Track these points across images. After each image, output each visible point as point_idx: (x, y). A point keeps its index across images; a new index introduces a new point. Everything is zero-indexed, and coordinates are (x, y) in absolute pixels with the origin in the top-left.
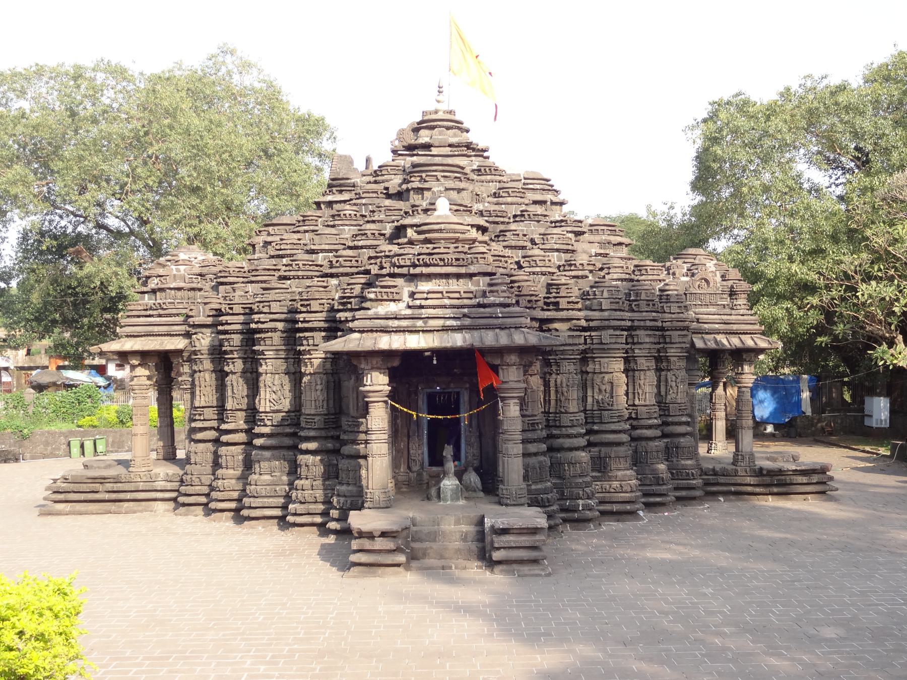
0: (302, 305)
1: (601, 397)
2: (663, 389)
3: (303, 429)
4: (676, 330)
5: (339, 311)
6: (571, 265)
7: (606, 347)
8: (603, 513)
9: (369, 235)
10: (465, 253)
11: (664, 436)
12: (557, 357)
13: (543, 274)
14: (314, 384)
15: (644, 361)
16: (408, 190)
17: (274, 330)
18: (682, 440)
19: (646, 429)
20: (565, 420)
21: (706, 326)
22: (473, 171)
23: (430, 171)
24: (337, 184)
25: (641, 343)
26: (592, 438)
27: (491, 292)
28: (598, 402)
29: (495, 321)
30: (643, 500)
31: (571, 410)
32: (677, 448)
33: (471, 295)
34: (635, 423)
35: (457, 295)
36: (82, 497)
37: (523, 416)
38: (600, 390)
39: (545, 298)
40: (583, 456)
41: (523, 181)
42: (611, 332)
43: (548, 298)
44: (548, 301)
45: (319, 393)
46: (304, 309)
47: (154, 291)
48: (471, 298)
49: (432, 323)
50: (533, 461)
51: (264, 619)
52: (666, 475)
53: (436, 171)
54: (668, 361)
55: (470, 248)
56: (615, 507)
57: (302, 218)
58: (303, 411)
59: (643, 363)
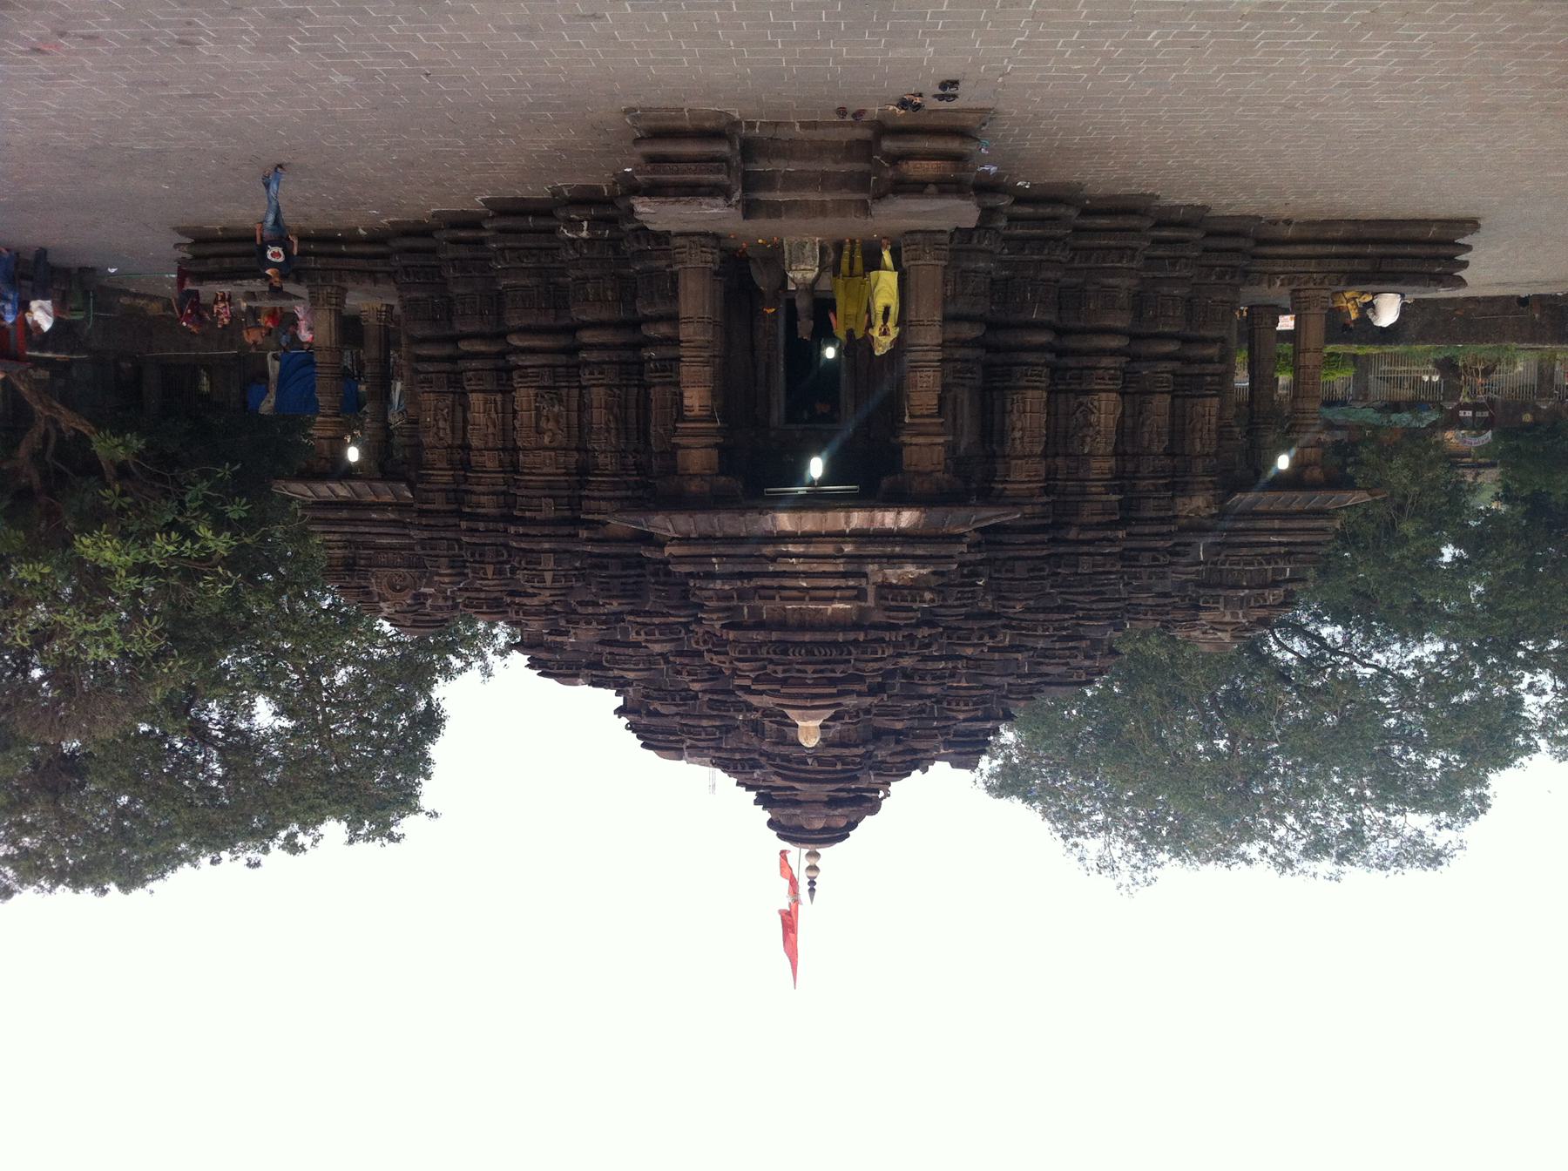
1: (556, 409)
2: (459, 415)
3: (1047, 365)
4: (438, 511)
5: (981, 562)
7: (547, 492)
9: (928, 677)
10: (771, 661)
13: (649, 614)
15: (488, 464)
16: (865, 742)
17: (1084, 527)
19: (482, 353)
22: (761, 767)
23: (829, 772)
25: (493, 493)
27: (729, 598)
28: (560, 401)
29: (722, 550)
30: (483, 234)
31: (602, 390)
32: (435, 320)
33: (762, 592)
34: (501, 363)
36: (1409, 250)
37: (677, 384)
38: (558, 422)
42: (539, 516)
44: (639, 571)
45: (1019, 425)
47: (1275, 584)
48: (764, 587)
49: (829, 549)
50: (662, 309)
51: (1148, 34)
53: (820, 772)
54: (450, 462)
59: (490, 461)
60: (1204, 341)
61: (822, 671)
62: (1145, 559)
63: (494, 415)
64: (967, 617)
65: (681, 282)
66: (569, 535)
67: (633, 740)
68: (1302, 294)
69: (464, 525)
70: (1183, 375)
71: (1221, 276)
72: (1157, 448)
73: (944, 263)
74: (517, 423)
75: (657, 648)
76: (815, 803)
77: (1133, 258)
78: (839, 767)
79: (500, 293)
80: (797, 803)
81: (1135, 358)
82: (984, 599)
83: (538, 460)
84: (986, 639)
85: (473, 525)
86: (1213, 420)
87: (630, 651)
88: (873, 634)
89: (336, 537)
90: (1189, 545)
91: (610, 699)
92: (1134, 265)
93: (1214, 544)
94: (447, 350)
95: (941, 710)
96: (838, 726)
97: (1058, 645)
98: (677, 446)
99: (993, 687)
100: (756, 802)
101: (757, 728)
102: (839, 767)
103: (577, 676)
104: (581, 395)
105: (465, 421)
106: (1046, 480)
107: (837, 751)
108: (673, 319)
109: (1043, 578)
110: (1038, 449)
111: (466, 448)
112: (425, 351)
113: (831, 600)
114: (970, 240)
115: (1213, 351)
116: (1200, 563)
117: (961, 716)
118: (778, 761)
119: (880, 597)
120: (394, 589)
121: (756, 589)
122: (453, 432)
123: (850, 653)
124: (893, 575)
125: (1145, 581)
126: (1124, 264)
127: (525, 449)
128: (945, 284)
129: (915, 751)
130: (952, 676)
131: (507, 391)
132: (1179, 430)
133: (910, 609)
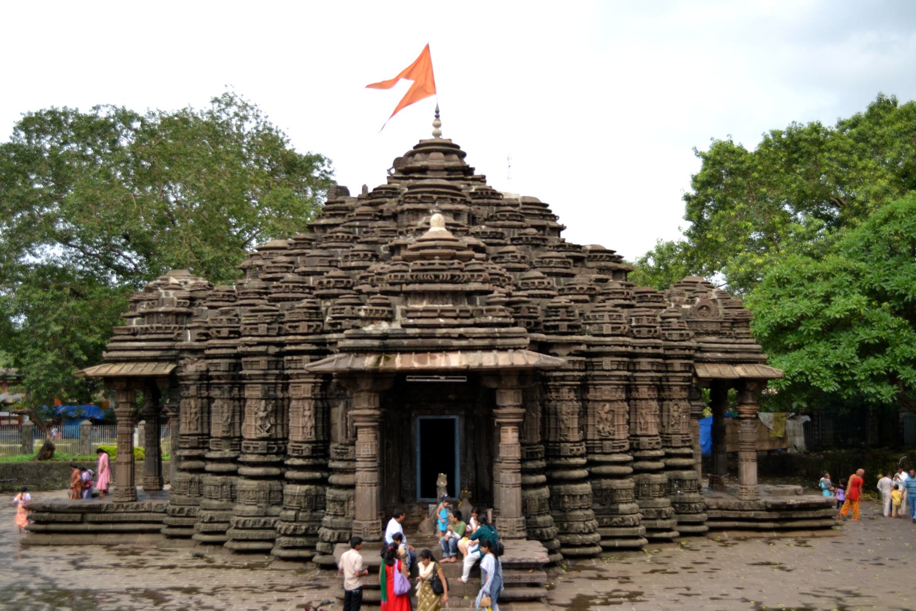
0: (290, 327)
3: (290, 457)
5: (328, 332)
6: (570, 289)
8: (606, 549)
10: (462, 270)
11: (592, 477)
12: (557, 383)
14: (301, 410)
15: (646, 390)
16: (402, 212)
18: (562, 487)
20: (566, 448)
21: (708, 355)
22: (471, 194)
24: (333, 209)
26: (594, 469)
27: (487, 311)
28: (599, 432)
34: (638, 454)
35: (453, 314)
37: (522, 445)
39: (544, 321)
40: (586, 487)
41: (521, 206)
43: (548, 321)
44: (548, 324)
45: (306, 419)
46: (292, 331)
48: (467, 318)
50: (532, 493)
52: (669, 510)
55: (466, 266)
56: (617, 543)
57: (294, 241)
58: (290, 438)
60: (191, 471)
61: (430, 264)
62: (225, 332)
63: (642, 421)
64: (336, 296)
65: (519, 509)
66: (593, 346)
67: (554, 209)
68: (130, 499)
69: (661, 351)
70: (203, 448)
71: (181, 510)
72: (217, 403)
73: (355, 521)
74: (627, 417)
75: (537, 273)
76: (435, 172)
77: (237, 522)
78: (419, 196)
79: (637, 498)
80: (447, 169)
81: (234, 460)
82: (327, 308)
83: (614, 394)
84: (325, 281)
85: (656, 351)
86: (183, 420)
87: (554, 270)
88: (397, 288)
89: (744, 341)
90: (197, 341)
91: (568, 236)
92: (236, 519)
93: (181, 341)
94: (670, 461)
95: (354, 233)
96: (420, 223)
97: (279, 275)
98: (521, 407)
99: (321, 248)
100: (473, 169)
101: (473, 220)
102: (419, 196)
103: (591, 251)
104: (585, 434)
105: (661, 416)
106: (288, 384)
107: (421, 206)
108: (525, 486)
109: (290, 321)
110: (294, 403)
111: (661, 400)
112: (686, 462)
113: (425, 311)
114: (339, 536)
115: (186, 464)
116: (189, 328)
117: (340, 228)
118: (459, 199)
119: (392, 312)
120: (708, 308)
121: (472, 316)
122: (669, 410)
123: (412, 276)
124: (384, 326)
125: (224, 318)
126: (243, 519)
127: (622, 401)
128: (354, 508)
129: (370, 205)
130: (346, 256)
131: (633, 436)
132: (206, 412)
133: (374, 304)
